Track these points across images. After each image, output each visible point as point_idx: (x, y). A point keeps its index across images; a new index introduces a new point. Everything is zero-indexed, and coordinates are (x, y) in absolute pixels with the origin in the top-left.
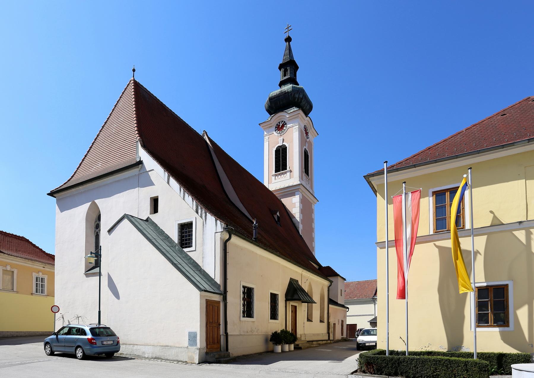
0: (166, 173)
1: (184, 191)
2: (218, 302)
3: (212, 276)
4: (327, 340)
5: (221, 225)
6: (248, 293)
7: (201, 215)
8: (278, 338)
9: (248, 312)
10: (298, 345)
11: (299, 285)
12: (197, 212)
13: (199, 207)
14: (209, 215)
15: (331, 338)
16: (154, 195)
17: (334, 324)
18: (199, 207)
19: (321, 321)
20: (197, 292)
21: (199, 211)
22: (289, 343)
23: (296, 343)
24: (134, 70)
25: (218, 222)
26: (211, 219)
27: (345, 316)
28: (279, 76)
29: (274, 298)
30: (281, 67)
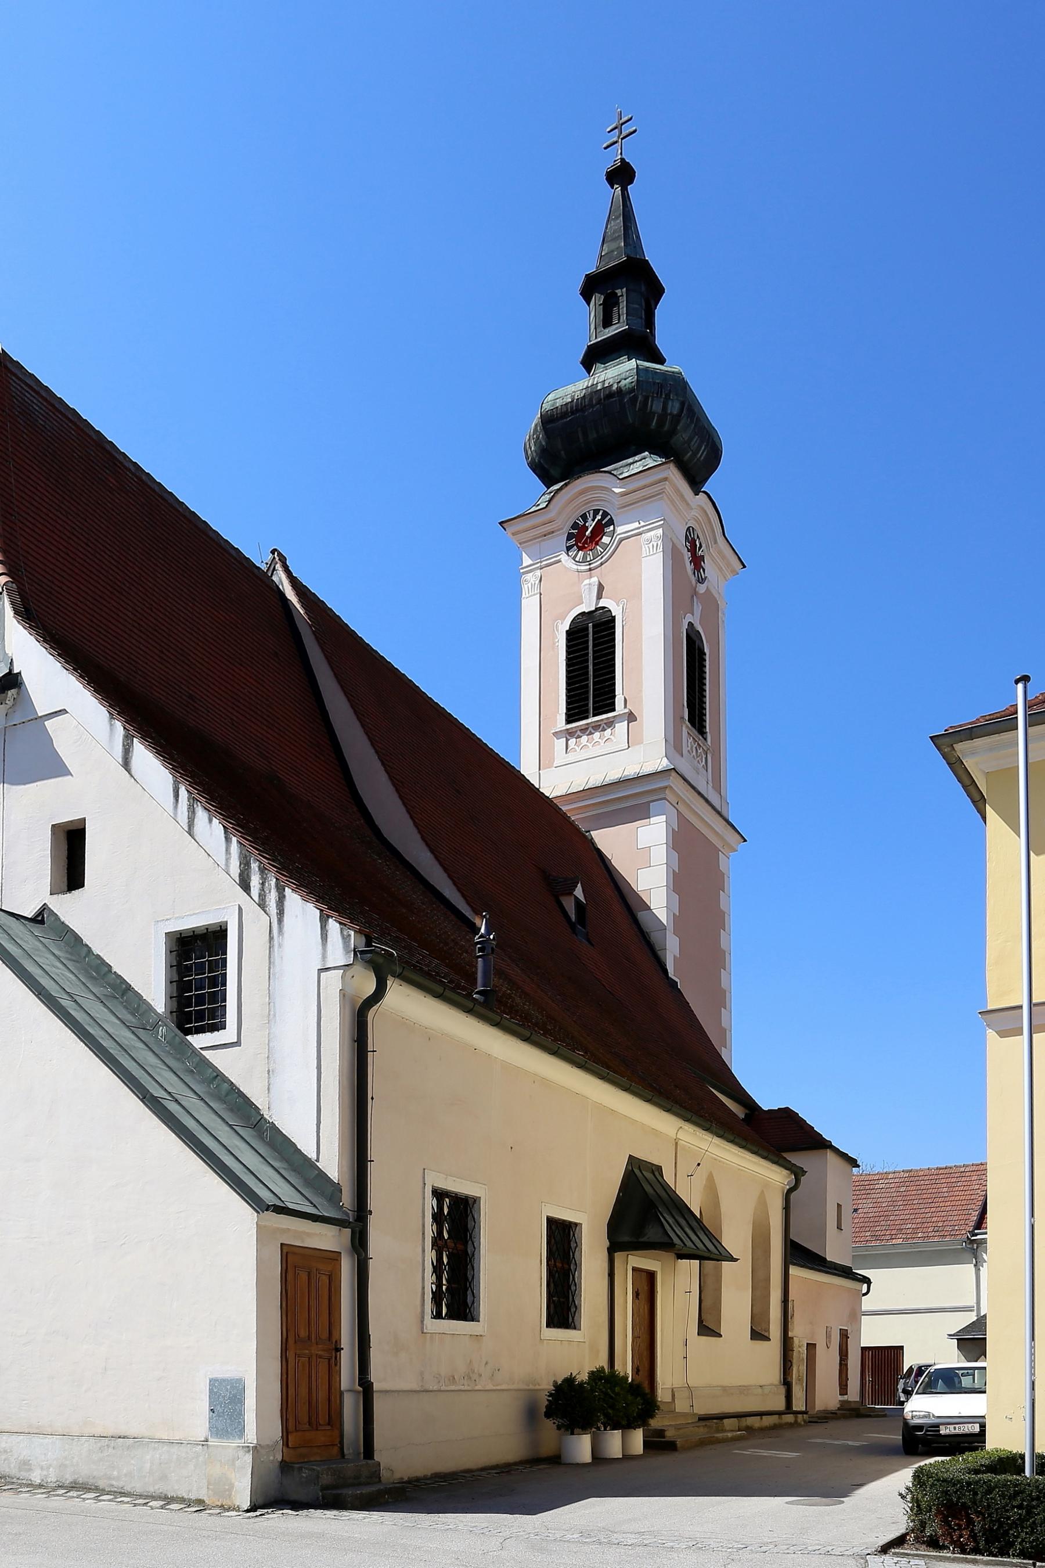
0: (119, 726)
1: (193, 800)
2: (334, 1257)
3: (307, 1147)
5: (345, 939)
6: (456, 1221)
7: (262, 896)
8: (577, 1404)
10: (661, 1433)
11: (665, 1187)
12: (245, 885)
13: (255, 866)
14: (293, 899)
15: (799, 1405)
21: (255, 881)
22: (625, 1424)
23: (655, 1423)
25: (333, 926)
26: (302, 912)
27: (856, 1315)
29: (561, 1237)
30: (591, 287)
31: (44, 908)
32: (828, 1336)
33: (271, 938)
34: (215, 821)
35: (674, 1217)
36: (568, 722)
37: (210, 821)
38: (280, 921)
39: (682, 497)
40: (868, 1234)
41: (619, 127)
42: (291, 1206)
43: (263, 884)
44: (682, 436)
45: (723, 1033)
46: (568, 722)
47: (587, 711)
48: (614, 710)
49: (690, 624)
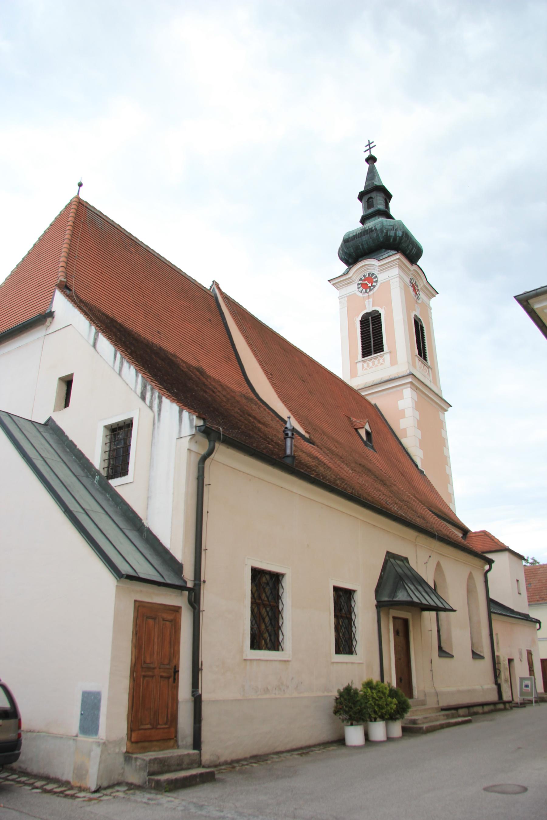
0: (93, 328)
1: (122, 358)
2: (177, 610)
3: (166, 542)
4: (494, 704)
5: (191, 421)
6: (266, 587)
7: (151, 402)
8: (352, 706)
9: (266, 631)
10: (414, 722)
11: (410, 569)
12: (143, 398)
13: (149, 387)
14: (166, 401)
15: (506, 697)
16: (65, 373)
17: (510, 661)
18: (149, 387)
19: (476, 655)
20: (109, 580)
21: (148, 395)
22: (390, 717)
23: (408, 716)
24: (80, 185)
25: (186, 414)
26: (170, 408)
27: (534, 642)
28: (358, 209)
29: (343, 598)
30: (361, 196)
31: (50, 419)
32: (521, 654)
33: (154, 424)
34: (132, 367)
35: (415, 586)
36: (363, 357)
37: (130, 368)
38: (159, 414)
39: (406, 266)
40: (538, 597)
41: (369, 144)
42: (142, 576)
43: (152, 396)
44: (404, 245)
45: (451, 495)
46: (363, 357)
47: (371, 352)
48: (383, 351)
49: (415, 316)
